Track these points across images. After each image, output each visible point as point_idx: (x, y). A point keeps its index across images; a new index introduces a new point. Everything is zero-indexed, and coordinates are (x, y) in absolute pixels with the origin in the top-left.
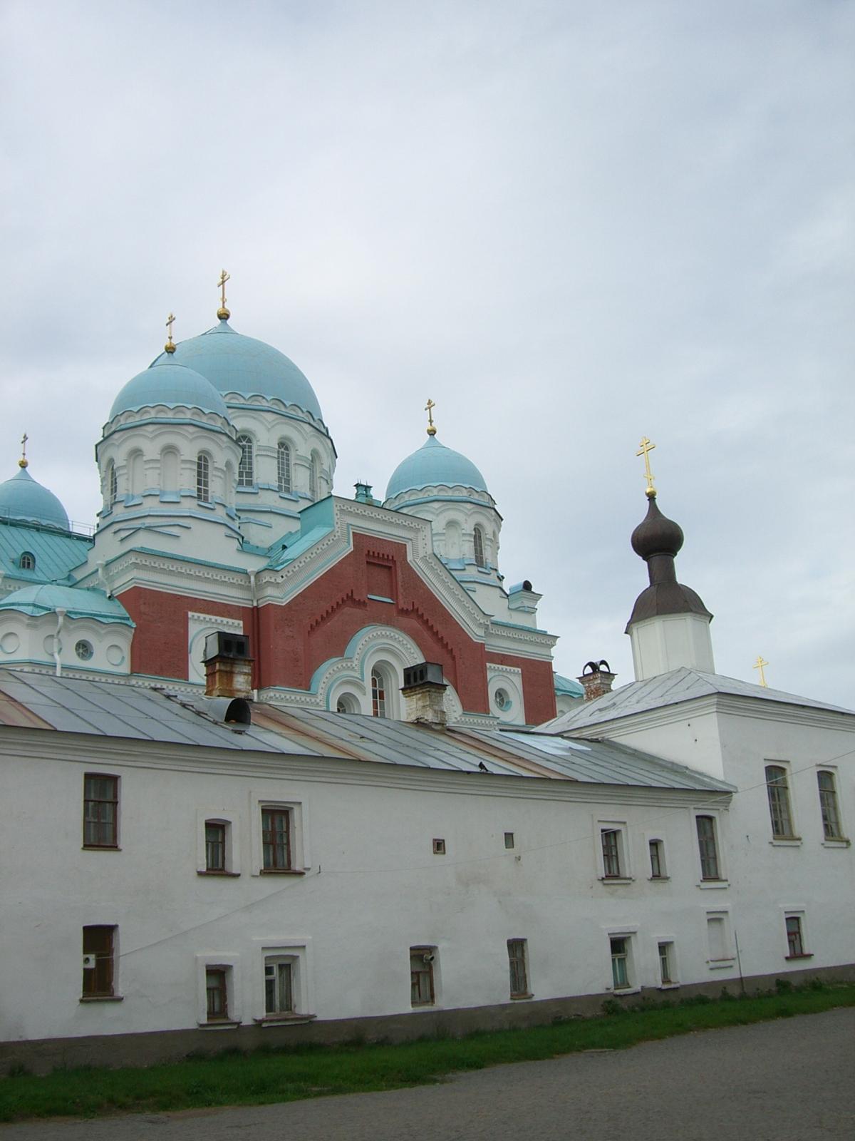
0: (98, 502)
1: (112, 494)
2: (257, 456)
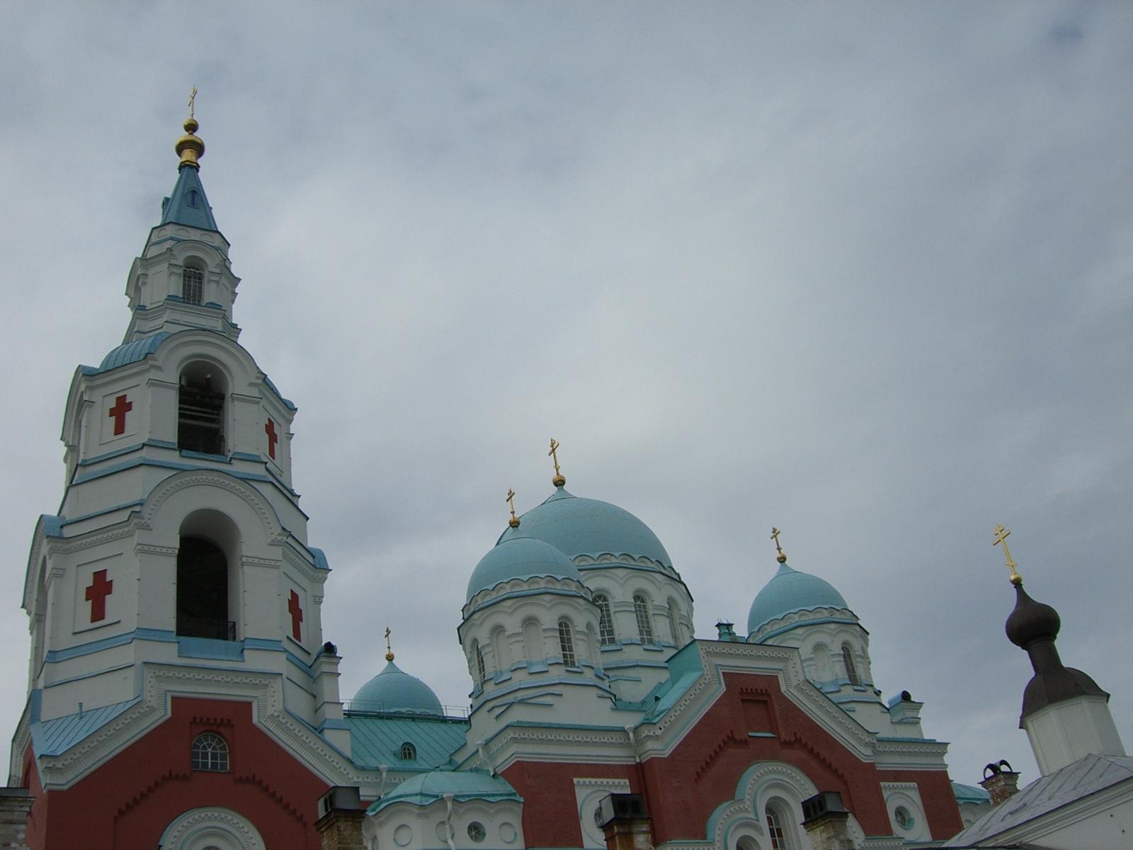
0: (468, 683)
1: (480, 673)
2: (615, 612)
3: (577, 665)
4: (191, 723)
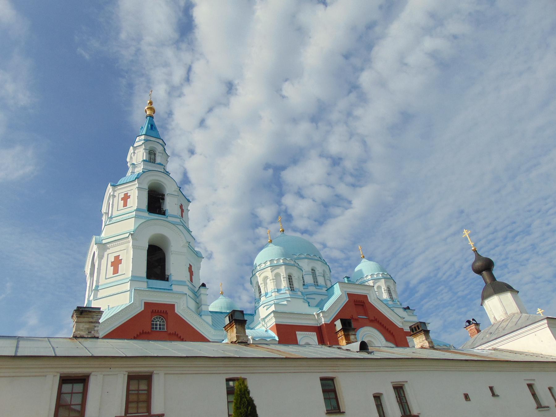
1: (259, 294)
2: (318, 276)
3: (295, 291)
4: (151, 312)
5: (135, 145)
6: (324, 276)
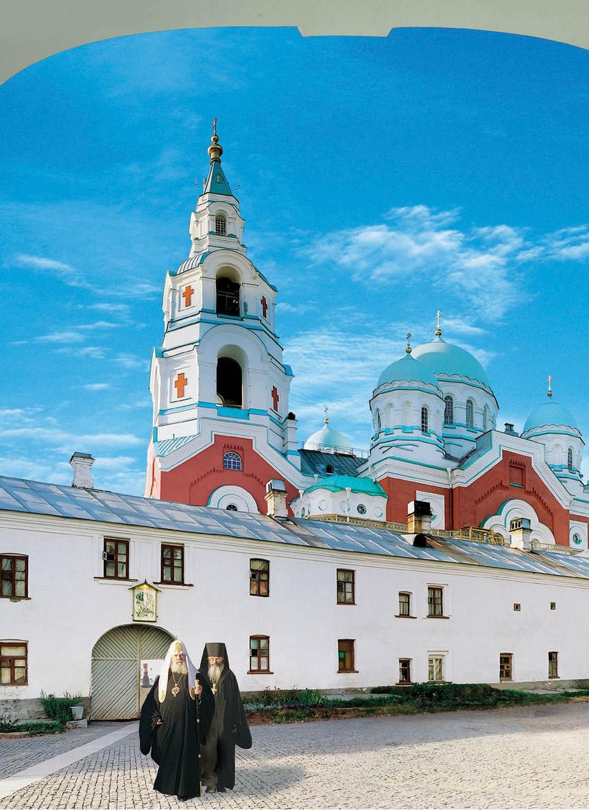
5: (198, 210)
6: (484, 415)
